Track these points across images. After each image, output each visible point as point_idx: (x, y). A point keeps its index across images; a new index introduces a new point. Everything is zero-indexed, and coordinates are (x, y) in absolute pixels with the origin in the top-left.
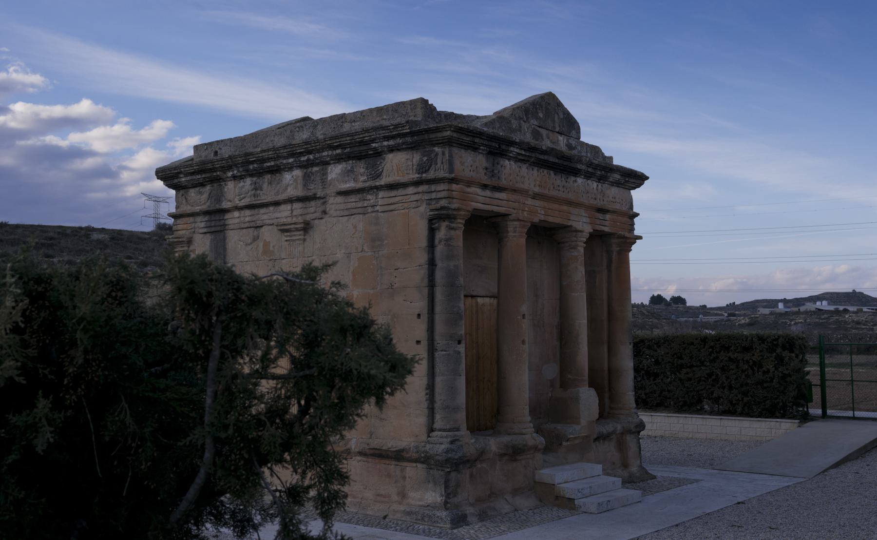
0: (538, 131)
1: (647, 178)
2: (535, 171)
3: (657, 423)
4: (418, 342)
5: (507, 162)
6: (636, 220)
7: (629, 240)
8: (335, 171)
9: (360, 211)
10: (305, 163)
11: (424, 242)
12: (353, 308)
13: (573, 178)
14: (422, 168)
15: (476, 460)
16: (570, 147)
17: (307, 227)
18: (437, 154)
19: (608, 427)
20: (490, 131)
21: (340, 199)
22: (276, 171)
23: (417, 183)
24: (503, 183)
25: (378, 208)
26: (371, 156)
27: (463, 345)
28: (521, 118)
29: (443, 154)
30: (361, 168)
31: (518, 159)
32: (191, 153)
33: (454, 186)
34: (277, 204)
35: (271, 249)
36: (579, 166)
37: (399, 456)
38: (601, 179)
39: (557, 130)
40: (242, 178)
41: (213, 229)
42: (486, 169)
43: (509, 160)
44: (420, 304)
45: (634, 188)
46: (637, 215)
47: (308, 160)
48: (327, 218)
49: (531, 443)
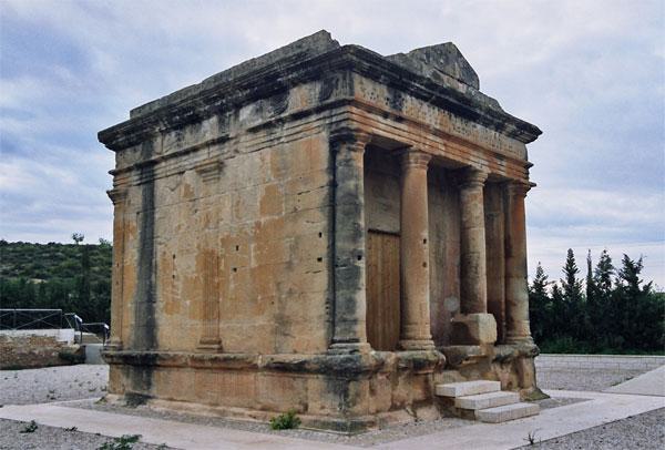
1: (541, 133)
2: (436, 109)
3: (545, 362)
4: (320, 260)
7: (524, 187)
8: (246, 113)
9: (268, 144)
11: (324, 163)
13: (473, 123)
14: (325, 95)
15: (376, 372)
17: (220, 166)
19: (505, 350)
21: (249, 137)
22: (196, 120)
23: (318, 110)
24: (404, 114)
25: (282, 140)
26: (277, 92)
27: (363, 260)
28: (423, 60)
30: (267, 105)
31: (418, 95)
32: (128, 118)
34: (195, 150)
36: (478, 111)
37: (300, 369)
38: (499, 128)
39: (458, 77)
40: (167, 131)
41: (144, 181)
43: (411, 95)
44: (321, 223)
45: (528, 142)
46: (532, 165)
48: (238, 156)
49: (432, 358)
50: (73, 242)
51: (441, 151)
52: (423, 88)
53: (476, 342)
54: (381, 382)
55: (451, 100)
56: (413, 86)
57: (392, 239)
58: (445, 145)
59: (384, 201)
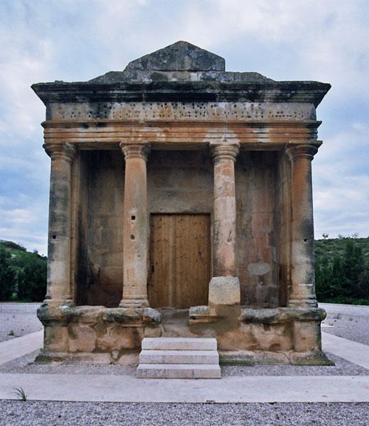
33: (51, 130)
42: (91, 113)
50: (323, 238)
51: (160, 136)
52: (125, 92)
53: (206, 303)
54: (83, 330)
55: (165, 92)
56: (113, 94)
57: (203, 218)
58: (165, 132)
59: (167, 189)
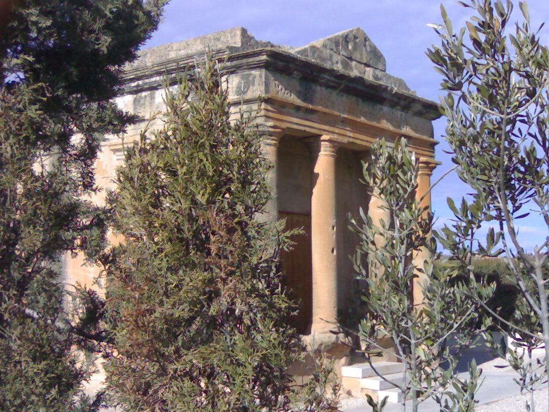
0: (305, 100)
5: (318, 88)
6: (436, 147)
10: (135, 89)
12: (5, 377)
13: (379, 106)
16: (376, 78)
18: (254, 77)
20: (303, 58)
29: (261, 76)
31: (327, 86)
35: (104, 168)
45: (435, 119)
47: (138, 86)
